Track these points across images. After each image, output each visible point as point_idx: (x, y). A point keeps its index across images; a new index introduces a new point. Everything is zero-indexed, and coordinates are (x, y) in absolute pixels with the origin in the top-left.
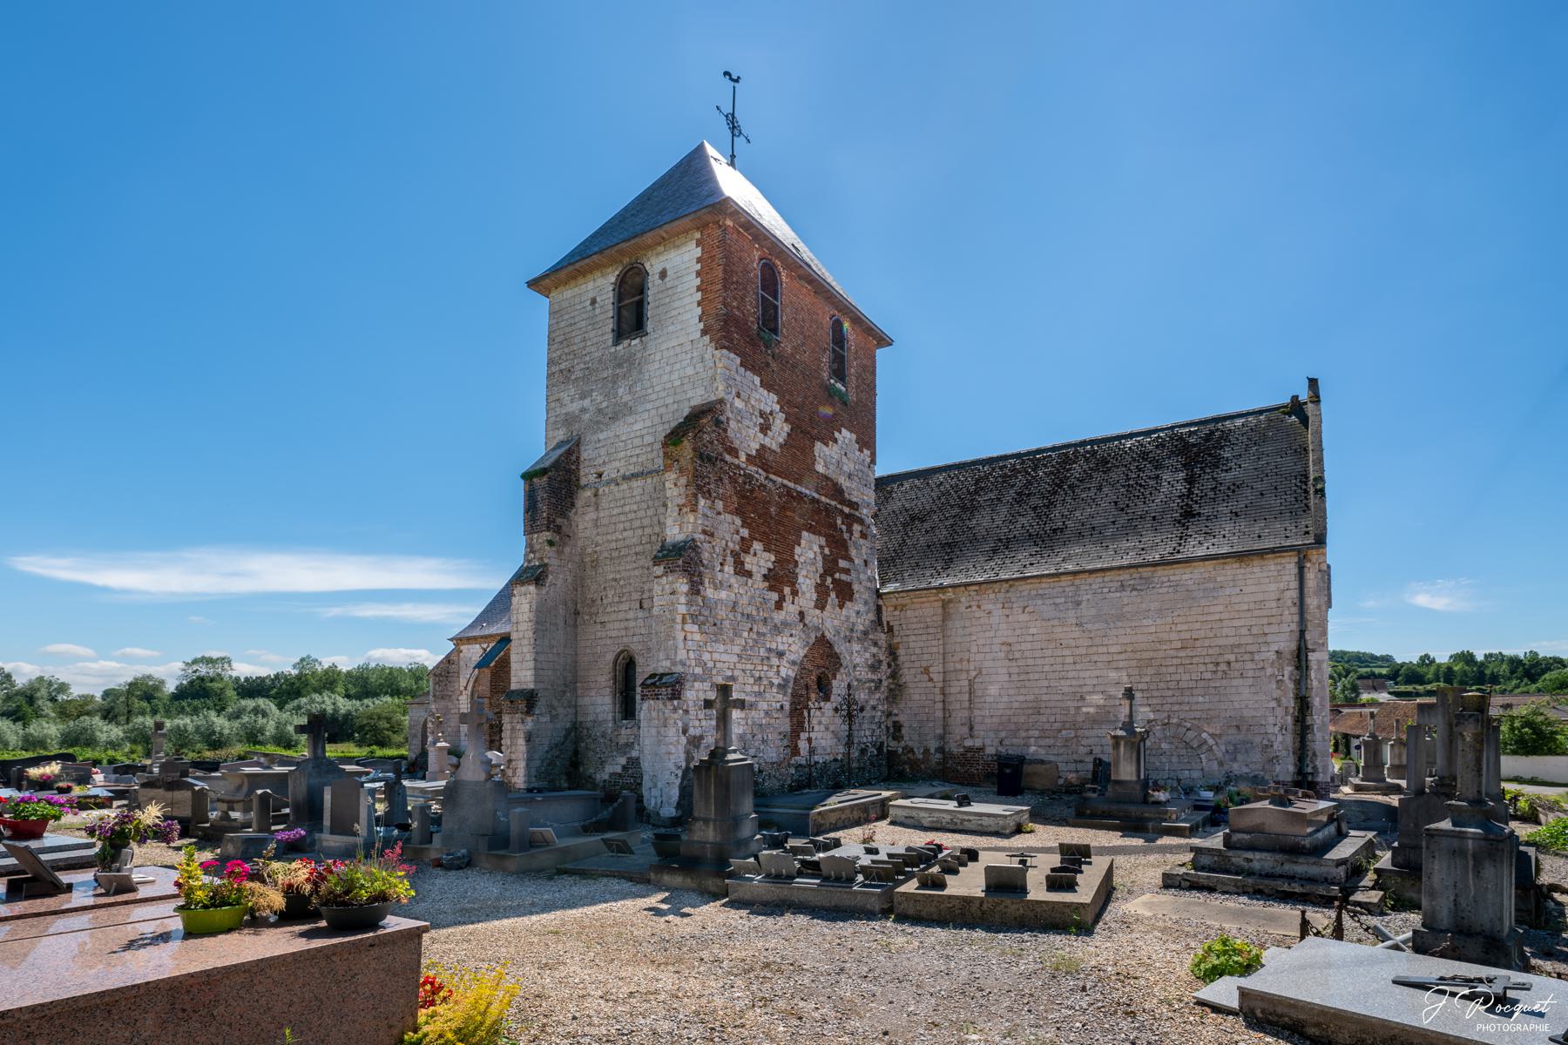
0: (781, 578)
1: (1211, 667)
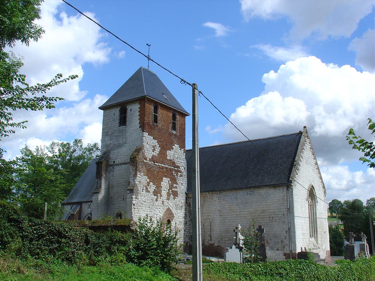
0: (157, 193)
1: (269, 219)
